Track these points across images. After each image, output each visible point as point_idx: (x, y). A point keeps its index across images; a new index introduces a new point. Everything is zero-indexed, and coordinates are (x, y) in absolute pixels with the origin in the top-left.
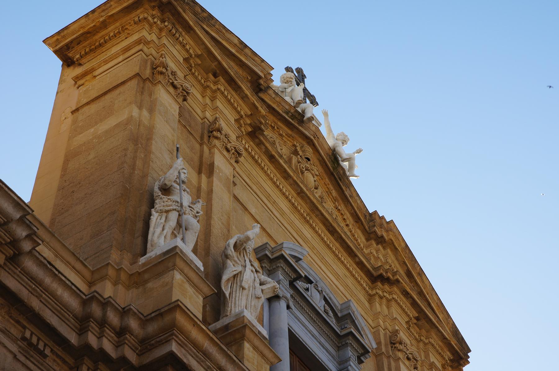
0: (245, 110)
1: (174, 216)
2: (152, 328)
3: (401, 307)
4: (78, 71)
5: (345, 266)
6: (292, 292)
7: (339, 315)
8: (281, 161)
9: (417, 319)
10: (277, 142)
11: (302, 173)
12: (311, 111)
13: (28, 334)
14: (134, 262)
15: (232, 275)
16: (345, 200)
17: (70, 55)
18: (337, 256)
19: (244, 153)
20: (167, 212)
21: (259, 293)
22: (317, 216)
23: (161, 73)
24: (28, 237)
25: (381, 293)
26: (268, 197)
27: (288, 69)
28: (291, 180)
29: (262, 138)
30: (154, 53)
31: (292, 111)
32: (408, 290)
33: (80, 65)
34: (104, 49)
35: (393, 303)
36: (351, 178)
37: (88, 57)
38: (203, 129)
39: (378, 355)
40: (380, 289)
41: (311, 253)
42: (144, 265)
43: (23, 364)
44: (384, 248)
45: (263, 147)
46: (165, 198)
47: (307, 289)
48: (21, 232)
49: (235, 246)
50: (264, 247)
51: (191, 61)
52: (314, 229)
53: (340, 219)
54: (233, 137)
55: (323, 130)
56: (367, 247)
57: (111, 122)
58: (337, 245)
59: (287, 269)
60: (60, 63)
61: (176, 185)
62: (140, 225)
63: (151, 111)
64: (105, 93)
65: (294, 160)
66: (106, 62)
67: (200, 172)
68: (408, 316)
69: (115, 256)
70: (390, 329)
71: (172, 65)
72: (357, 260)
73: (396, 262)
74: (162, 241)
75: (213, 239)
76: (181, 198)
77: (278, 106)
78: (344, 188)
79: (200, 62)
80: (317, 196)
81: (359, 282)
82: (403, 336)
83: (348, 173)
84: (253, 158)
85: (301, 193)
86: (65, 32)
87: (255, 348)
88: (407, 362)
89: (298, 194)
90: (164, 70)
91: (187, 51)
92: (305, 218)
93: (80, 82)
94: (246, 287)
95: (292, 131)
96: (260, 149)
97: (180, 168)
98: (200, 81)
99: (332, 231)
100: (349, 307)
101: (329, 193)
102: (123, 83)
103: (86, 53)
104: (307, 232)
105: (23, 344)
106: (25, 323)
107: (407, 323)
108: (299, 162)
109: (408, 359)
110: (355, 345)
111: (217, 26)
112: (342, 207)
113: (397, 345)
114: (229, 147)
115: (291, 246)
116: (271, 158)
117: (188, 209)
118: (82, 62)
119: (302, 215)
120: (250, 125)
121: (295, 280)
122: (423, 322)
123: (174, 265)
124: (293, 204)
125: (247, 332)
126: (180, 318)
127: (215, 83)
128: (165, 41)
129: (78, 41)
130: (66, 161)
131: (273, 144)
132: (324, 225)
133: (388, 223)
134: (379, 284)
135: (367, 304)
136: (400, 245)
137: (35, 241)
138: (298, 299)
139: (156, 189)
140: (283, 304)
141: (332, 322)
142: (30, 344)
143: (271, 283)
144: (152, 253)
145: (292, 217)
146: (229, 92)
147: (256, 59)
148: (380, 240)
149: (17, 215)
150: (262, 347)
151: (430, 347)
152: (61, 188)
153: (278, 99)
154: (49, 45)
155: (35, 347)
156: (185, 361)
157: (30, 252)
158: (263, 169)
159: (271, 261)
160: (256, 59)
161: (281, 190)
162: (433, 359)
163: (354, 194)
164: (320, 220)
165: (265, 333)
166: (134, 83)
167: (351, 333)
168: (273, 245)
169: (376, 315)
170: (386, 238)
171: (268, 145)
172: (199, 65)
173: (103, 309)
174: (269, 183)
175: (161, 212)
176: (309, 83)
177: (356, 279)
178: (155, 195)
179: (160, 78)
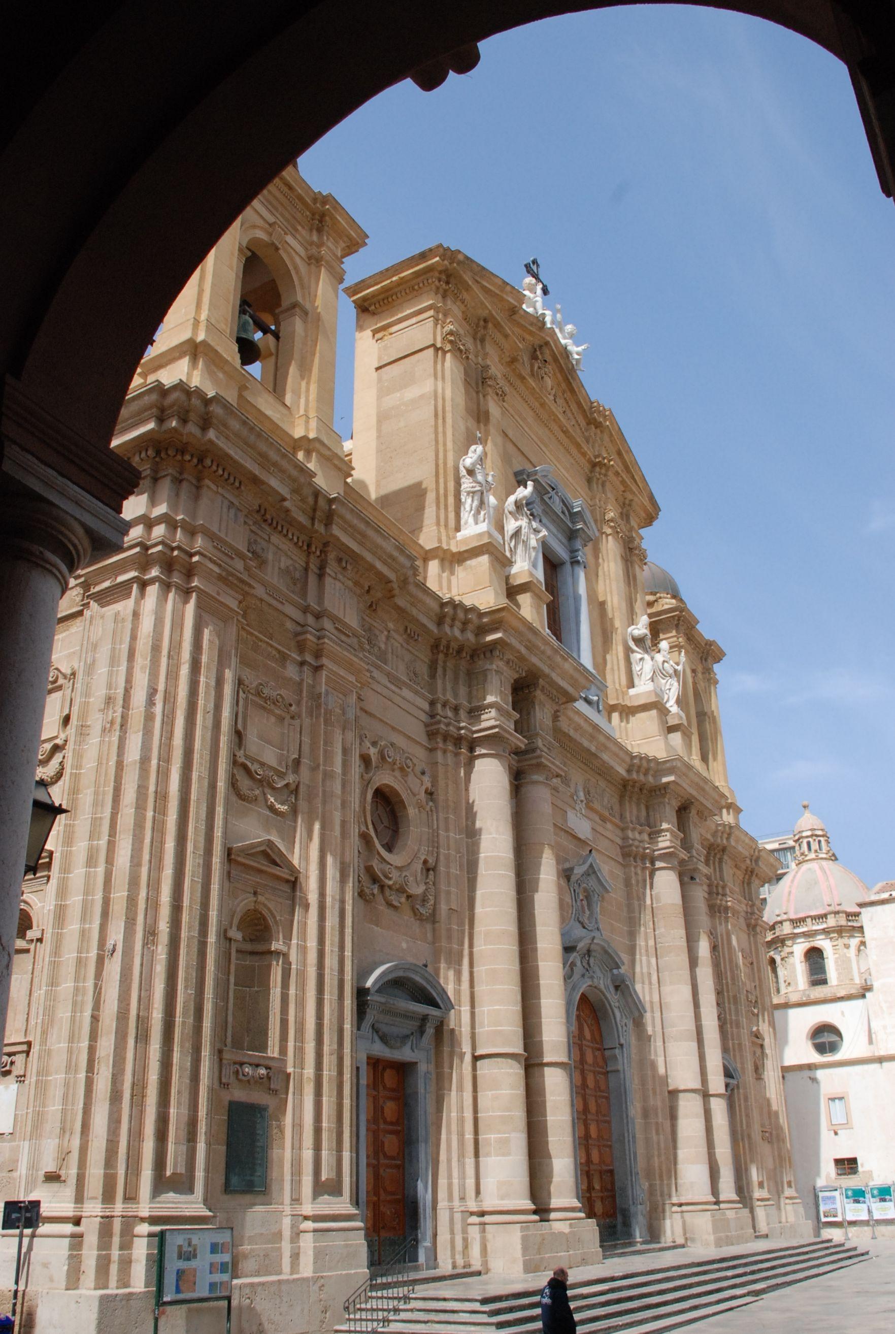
11: (542, 378)
16: (572, 391)
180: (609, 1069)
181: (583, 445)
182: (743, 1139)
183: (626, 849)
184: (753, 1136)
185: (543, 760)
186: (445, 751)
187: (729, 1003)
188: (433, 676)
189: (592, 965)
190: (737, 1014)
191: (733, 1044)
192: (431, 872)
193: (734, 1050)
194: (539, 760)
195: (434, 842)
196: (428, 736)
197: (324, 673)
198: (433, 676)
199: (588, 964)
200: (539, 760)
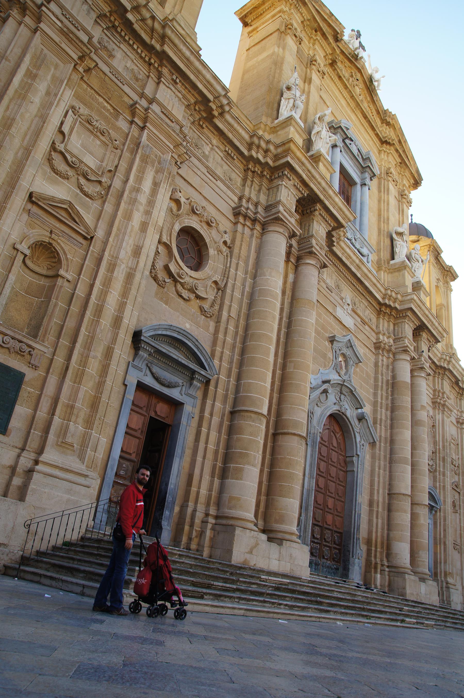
0: (329, 51)
1: (291, 101)
2: (280, 150)
3: (394, 157)
4: (250, 29)
5: (369, 135)
6: (343, 144)
7: (364, 158)
8: (344, 80)
9: (401, 163)
10: (343, 70)
11: (354, 87)
12: (361, 53)
13: (227, 149)
14: (272, 122)
15: (316, 132)
16: (373, 102)
17: (246, 20)
18: (366, 130)
19: (327, 75)
20: (289, 99)
21: (328, 141)
22: (359, 109)
23: (290, 29)
24: (228, 104)
25: (385, 150)
26: (336, 97)
27: (353, 30)
28: (348, 90)
29: (336, 67)
30: (287, 18)
31: (353, 53)
32: (398, 149)
33: (251, 25)
34: (262, 16)
35: (390, 155)
36: (378, 91)
37: (255, 21)
38: (308, 60)
39: (379, 179)
40: (385, 147)
41: (354, 127)
42: (277, 123)
43: (225, 162)
44: (389, 128)
45: (336, 72)
46: (288, 92)
47: (350, 144)
48: (225, 102)
49: (319, 118)
50: (332, 122)
51: (305, 23)
52: (357, 115)
53: (370, 112)
54: (322, 65)
55: (367, 65)
56: (381, 127)
57: (264, 55)
58: (367, 124)
59: (342, 133)
60: (242, 25)
61: (293, 86)
62: (276, 105)
63: (284, 49)
64: (262, 40)
65: (351, 79)
66: (263, 23)
67: (305, 82)
68: (396, 161)
69: (264, 119)
70: (387, 167)
71: (295, 25)
72: (376, 132)
73: (394, 135)
74: (286, 112)
75: (309, 115)
76: (296, 93)
77: (346, 50)
78: (373, 96)
79: (309, 24)
80: (360, 99)
81: (375, 143)
82: (392, 170)
83: (376, 89)
84: (331, 77)
85: (352, 97)
86: (245, 7)
87: (324, 165)
88: (393, 182)
89: (351, 97)
90: (291, 27)
91: (303, 17)
92: (353, 110)
93: (251, 35)
94: (323, 138)
95: (351, 64)
96: (335, 72)
97: (296, 77)
98: (308, 35)
99: (365, 117)
100: (369, 154)
101: (366, 98)
102: (271, 34)
103: (254, 19)
104: (353, 117)
105: (225, 153)
106: (226, 144)
107: (396, 165)
108: (353, 81)
109: (394, 181)
110: (370, 172)
111: (319, 3)
112: (371, 106)
113: (389, 174)
114: (319, 69)
115: (345, 122)
116: (340, 77)
117: (298, 98)
118: (252, 24)
119: (352, 108)
120: (331, 59)
121: (345, 139)
122: (403, 165)
123: (291, 124)
124: (348, 102)
125: (322, 158)
126: (292, 146)
127: (316, 36)
128: (292, 11)
129: (250, 12)
130: (244, 75)
131: (341, 70)
132: (362, 114)
133: (393, 115)
134: (385, 145)
135: (378, 154)
136: (397, 127)
137: (231, 106)
138: (346, 148)
139: (284, 88)
140: (338, 149)
141: (360, 160)
142: (228, 154)
143: (334, 137)
144: (281, 118)
145: (347, 109)
146: (322, 41)
147: (337, 22)
148: (388, 124)
149: (223, 93)
150: (327, 165)
151: (404, 177)
152: (241, 88)
153: (346, 46)
154: (237, 15)
155: (230, 155)
156: (293, 165)
157: (228, 111)
158: (335, 83)
159: (335, 129)
160: (337, 22)
161: (343, 95)
162: (405, 182)
163: (378, 100)
164: (360, 111)
165: (329, 160)
166: (276, 34)
167: (369, 166)
168: (336, 121)
169: (381, 160)
170: (391, 123)
171: (339, 71)
172: (308, 25)
173: (259, 140)
174: (337, 91)
175: (286, 99)
176: (362, 39)
177: (374, 142)
178: (283, 91)
179: (289, 31)
180: (348, 469)
181: (426, 468)
182: (440, 544)
183: (377, 345)
184: (447, 543)
185: (313, 249)
186: (244, 225)
187: (439, 460)
188: (244, 185)
189: (342, 400)
190: (444, 468)
191: (440, 485)
192: (220, 291)
193: (440, 489)
194: (311, 249)
195: (226, 274)
196: (234, 216)
197: (146, 131)
198: (244, 185)
199: (340, 398)
200: (311, 249)
